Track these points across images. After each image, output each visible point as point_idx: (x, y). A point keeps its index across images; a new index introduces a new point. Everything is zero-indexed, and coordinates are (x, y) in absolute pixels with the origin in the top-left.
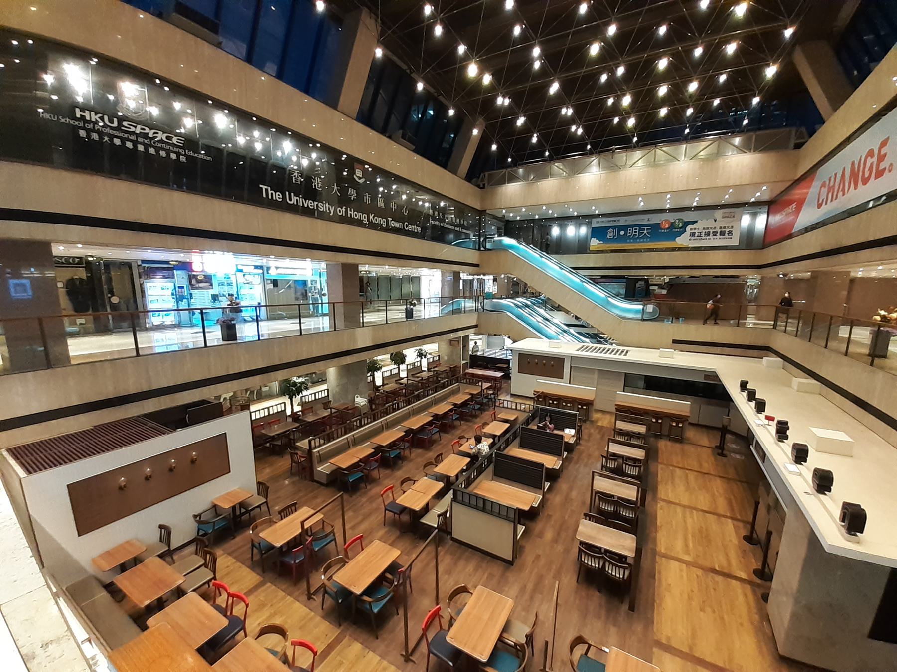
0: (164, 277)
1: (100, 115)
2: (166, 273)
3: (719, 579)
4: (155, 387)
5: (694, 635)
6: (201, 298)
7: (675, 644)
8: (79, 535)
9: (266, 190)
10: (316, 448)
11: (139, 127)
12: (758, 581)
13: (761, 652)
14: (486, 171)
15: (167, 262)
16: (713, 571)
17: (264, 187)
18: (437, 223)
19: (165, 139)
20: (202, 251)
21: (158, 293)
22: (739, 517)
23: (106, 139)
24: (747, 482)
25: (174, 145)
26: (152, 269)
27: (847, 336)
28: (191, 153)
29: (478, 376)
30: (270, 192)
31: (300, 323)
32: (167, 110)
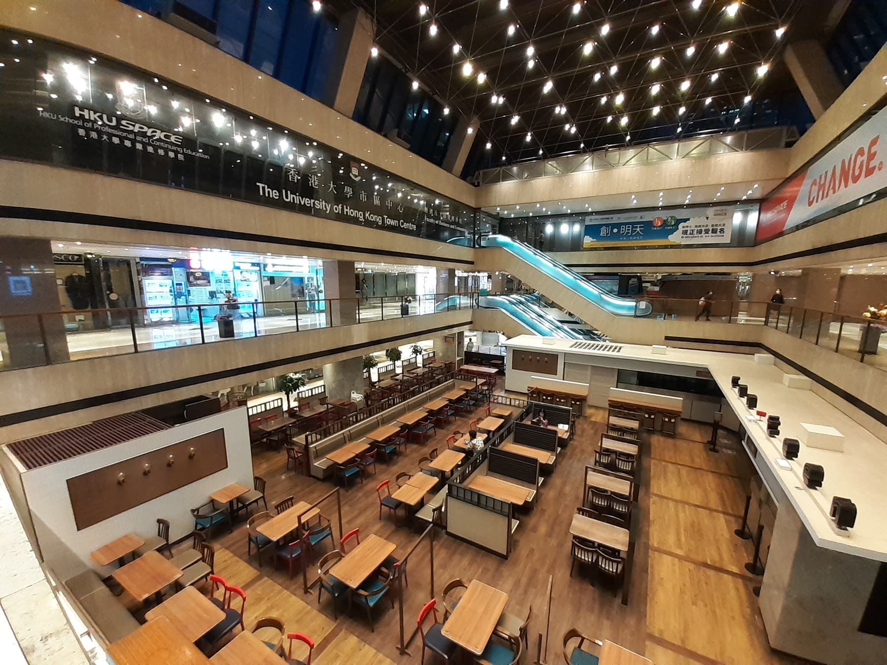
0: (162, 274)
1: (99, 114)
2: (164, 270)
3: (711, 573)
4: (153, 383)
5: (686, 629)
6: (199, 295)
7: (667, 637)
8: (78, 530)
9: (264, 188)
10: (312, 443)
11: (137, 125)
12: (750, 575)
13: (752, 645)
14: (480, 169)
15: (166, 260)
16: (705, 565)
17: (261, 185)
18: (432, 221)
19: (163, 138)
20: (200, 248)
21: (156, 290)
22: (730, 512)
23: (105, 137)
24: (739, 477)
25: (172, 144)
26: (150, 267)
27: (838, 332)
28: (189, 152)
29: (473, 372)
30: (267, 190)
31: (297, 320)
32: (165, 109)
